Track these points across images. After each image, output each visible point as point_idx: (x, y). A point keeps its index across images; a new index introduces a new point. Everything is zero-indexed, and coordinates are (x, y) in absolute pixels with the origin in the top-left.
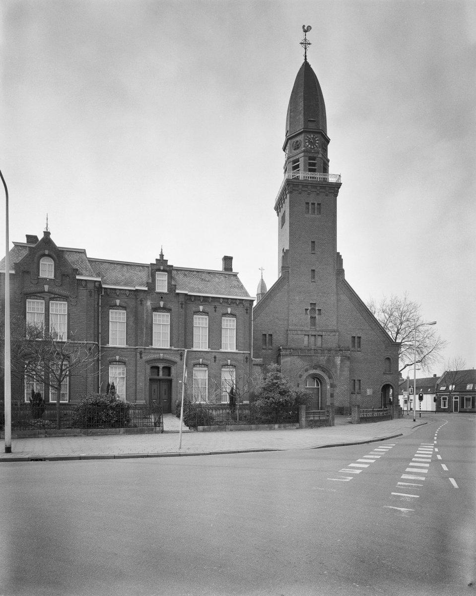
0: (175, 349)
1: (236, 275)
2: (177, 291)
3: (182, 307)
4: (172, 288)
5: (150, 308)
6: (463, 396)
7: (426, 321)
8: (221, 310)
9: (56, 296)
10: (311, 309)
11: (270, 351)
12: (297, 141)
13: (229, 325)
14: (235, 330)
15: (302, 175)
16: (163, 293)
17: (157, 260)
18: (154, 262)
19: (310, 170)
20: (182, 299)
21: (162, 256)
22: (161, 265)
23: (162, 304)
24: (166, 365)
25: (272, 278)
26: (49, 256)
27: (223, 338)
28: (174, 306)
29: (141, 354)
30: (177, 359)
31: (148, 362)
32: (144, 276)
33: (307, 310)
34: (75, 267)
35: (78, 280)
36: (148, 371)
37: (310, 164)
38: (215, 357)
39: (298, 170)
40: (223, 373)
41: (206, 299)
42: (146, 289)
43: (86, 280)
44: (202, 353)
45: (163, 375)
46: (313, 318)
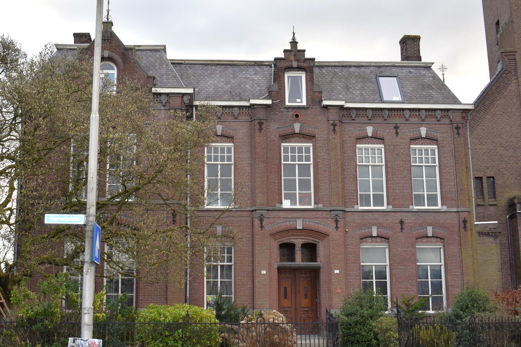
1: (430, 67)
2: (325, 103)
3: (334, 130)
4: (315, 97)
5: (275, 136)
8: (406, 132)
11: (492, 208)
13: (425, 158)
16: (299, 108)
17: (285, 51)
18: (282, 55)
20: (334, 115)
21: (294, 43)
22: (294, 59)
24: (309, 240)
25: (483, 79)
28: (322, 131)
29: (261, 220)
30: (328, 227)
31: (274, 235)
32: (262, 79)
34: (151, 73)
36: (276, 252)
38: (402, 222)
40: (419, 256)
42: (269, 102)
43: (168, 94)
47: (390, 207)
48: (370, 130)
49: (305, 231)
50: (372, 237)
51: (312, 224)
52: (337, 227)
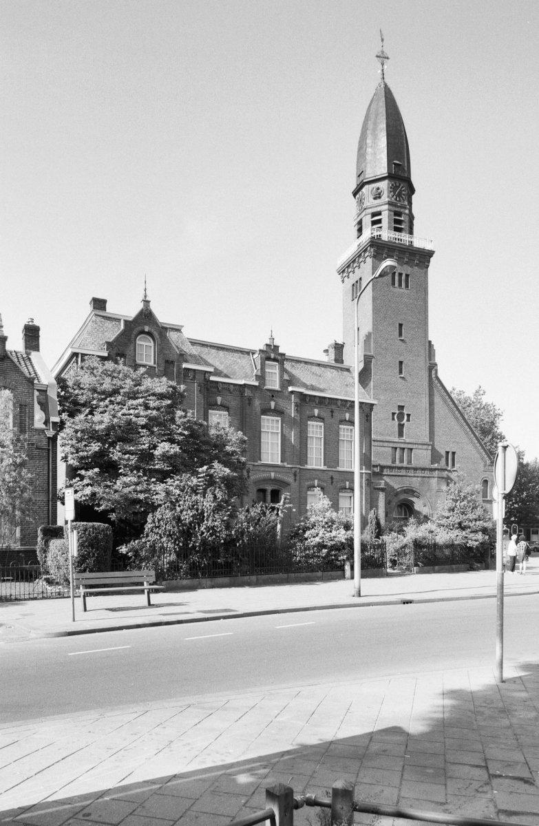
4: (285, 383)
5: (258, 410)
6: (528, 528)
7: (269, 380)
8: (337, 415)
10: (399, 413)
12: (378, 189)
14: (280, 435)
15: (386, 234)
16: (274, 391)
19: (397, 229)
22: (271, 354)
23: (273, 404)
24: (275, 487)
26: (149, 334)
27: (341, 454)
31: (256, 482)
33: (393, 414)
37: (397, 222)
38: (332, 478)
39: (381, 227)
41: (322, 400)
43: (194, 370)
44: (318, 473)
46: (401, 426)
47: (326, 467)
49: (275, 481)
51: (279, 476)
52: (295, 480)
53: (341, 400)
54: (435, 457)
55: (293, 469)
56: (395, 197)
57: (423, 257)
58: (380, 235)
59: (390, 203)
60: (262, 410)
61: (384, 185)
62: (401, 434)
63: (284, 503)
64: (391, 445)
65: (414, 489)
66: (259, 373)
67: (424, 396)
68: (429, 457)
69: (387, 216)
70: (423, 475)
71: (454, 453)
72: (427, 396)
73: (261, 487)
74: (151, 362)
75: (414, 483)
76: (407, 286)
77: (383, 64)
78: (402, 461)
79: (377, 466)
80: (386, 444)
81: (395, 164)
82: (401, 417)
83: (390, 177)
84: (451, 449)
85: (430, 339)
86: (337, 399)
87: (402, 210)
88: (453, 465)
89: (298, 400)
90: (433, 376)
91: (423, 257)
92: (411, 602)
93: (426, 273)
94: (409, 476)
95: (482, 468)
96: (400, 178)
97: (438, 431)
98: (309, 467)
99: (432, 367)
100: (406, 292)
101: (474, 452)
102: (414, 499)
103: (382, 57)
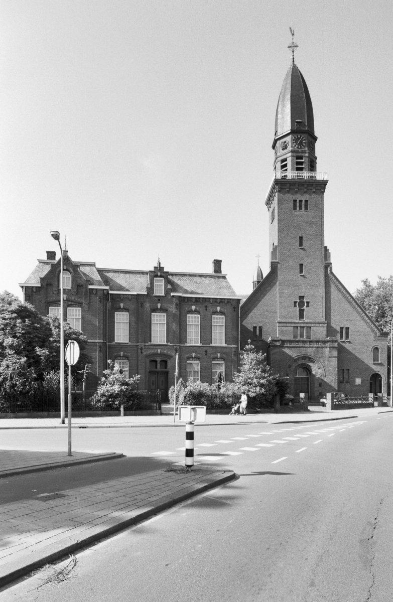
0: (171, 345)
5: (149, 310)
8: (211, 309)
9: (72, 303)
12: (285, 142)
13: (219, 322)
16: (160, 296)
17: (155, 267)
19: (298, 169)
22: (158, 272)
23: (159, 305)
31: (148, 356)
33: (295, 302)
35: (90, 289)
38: (206, 351)
39: (286, 170)
41: (197, 299)
43: (96, 289)
44: (195, 348)
45: (161, 368)
48: (218, 309)
49: (161, 354)
50: (192, 358)
51: (165, 352)
53: (213, 299)
54: (330, 331)
55: (205, 348)
56: (297, 146)
57: (321, 186)
58: (285, 176)
59: (292, 151)
60: (151, 309)
61: (288, 139)
62: (301, 315)
63: (87, 370)
64: (294, 325)
65: (310, 357)
66: (149, 286)
67: (321, 287)
68: (325, 332)
69: (290, 160)
70: (317, 346)
71: (347, 329)
72: (324, 287)
73: (152, 359)
74: (69, 286)
75: (310, 352)
76: (306, 208)
77: (293, 52)
78: (302, 336)
79: (278, 341)
80: (289, 325)
81: (297, 122)
82: (301, 304)
83: (293, 132)
84: (345, 324)
85: (325, 245)
86: (210, 298)
87: (303, 154)
88: (347, 337)
89: (177, 301)
90: (329, 272)
91: (321, 186)
92: (86, 428)
93: (322, 198)
94: (306, 347)
95: (373, 339)
96: (303, 131)
97: (334, 312)
98: (187, 344)
99: (328, 266)
100: (305, 213)
101: (365, 326)
102: (310, 364)
103: (293, 47)
